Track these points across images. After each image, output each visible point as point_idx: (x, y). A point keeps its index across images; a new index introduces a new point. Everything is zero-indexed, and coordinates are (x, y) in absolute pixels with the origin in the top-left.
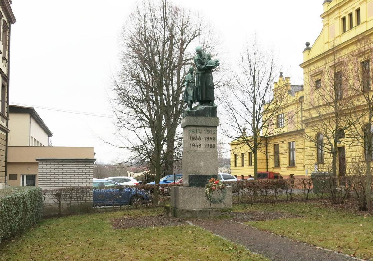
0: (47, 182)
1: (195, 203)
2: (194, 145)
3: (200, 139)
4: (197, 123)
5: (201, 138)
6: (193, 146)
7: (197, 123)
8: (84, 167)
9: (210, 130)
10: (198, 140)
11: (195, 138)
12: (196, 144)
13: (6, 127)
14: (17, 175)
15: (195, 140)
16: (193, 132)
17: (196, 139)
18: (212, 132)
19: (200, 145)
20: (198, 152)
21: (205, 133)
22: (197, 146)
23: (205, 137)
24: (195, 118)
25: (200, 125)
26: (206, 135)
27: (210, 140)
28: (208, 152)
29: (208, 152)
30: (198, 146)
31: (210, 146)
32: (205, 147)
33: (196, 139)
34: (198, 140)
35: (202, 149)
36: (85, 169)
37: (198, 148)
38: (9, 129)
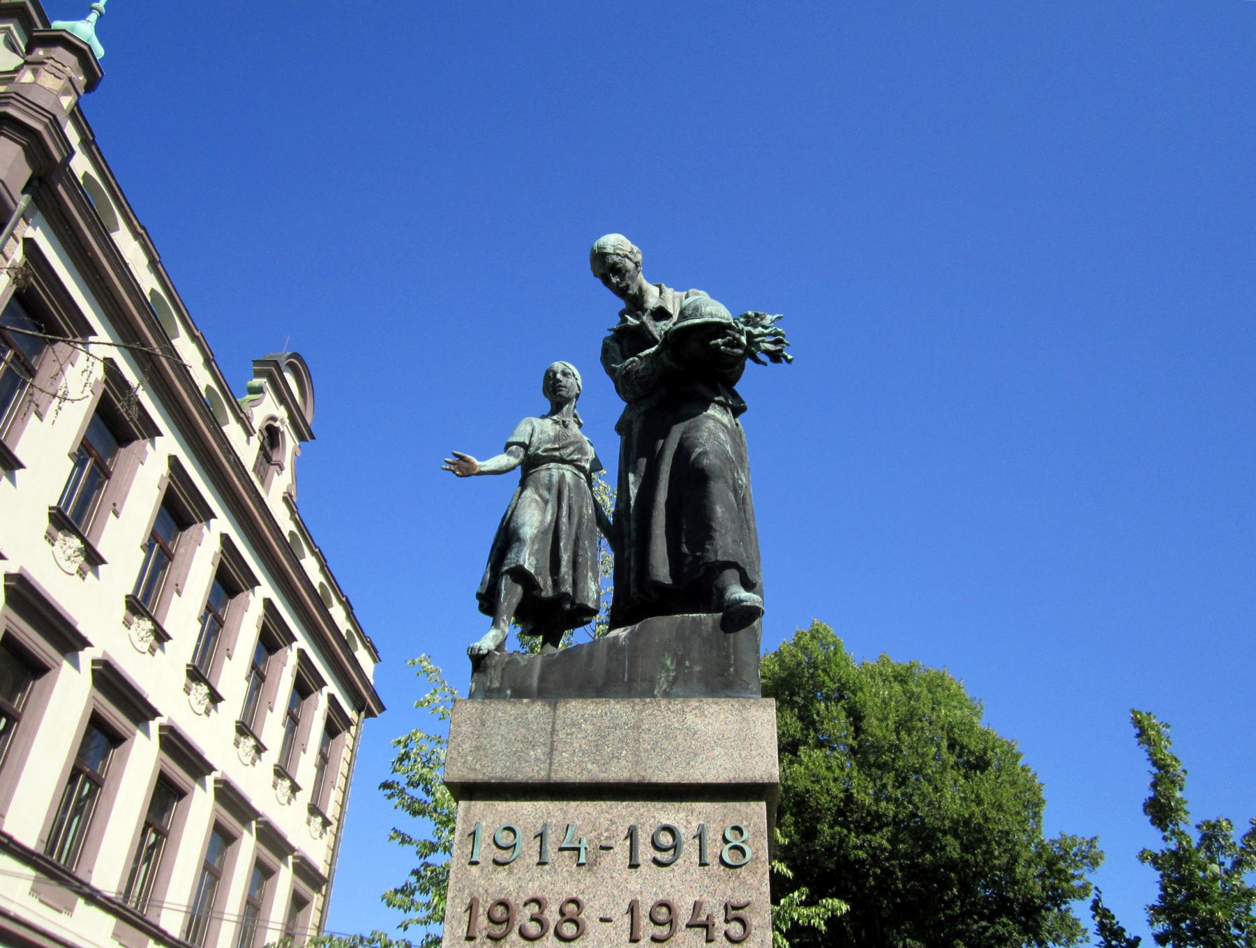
4: (550, 754)
5: (590, 915)
7: (550, 754)
9: (687, 833)
11: (524, 915)
15: (523, 934)
16: (503, 856)
17: (533, 929)
18: (714, 848)
23: (632, 909)
24: (536, 710)
25: (583, 777)
26: (648, 885)
33: (533, 929)
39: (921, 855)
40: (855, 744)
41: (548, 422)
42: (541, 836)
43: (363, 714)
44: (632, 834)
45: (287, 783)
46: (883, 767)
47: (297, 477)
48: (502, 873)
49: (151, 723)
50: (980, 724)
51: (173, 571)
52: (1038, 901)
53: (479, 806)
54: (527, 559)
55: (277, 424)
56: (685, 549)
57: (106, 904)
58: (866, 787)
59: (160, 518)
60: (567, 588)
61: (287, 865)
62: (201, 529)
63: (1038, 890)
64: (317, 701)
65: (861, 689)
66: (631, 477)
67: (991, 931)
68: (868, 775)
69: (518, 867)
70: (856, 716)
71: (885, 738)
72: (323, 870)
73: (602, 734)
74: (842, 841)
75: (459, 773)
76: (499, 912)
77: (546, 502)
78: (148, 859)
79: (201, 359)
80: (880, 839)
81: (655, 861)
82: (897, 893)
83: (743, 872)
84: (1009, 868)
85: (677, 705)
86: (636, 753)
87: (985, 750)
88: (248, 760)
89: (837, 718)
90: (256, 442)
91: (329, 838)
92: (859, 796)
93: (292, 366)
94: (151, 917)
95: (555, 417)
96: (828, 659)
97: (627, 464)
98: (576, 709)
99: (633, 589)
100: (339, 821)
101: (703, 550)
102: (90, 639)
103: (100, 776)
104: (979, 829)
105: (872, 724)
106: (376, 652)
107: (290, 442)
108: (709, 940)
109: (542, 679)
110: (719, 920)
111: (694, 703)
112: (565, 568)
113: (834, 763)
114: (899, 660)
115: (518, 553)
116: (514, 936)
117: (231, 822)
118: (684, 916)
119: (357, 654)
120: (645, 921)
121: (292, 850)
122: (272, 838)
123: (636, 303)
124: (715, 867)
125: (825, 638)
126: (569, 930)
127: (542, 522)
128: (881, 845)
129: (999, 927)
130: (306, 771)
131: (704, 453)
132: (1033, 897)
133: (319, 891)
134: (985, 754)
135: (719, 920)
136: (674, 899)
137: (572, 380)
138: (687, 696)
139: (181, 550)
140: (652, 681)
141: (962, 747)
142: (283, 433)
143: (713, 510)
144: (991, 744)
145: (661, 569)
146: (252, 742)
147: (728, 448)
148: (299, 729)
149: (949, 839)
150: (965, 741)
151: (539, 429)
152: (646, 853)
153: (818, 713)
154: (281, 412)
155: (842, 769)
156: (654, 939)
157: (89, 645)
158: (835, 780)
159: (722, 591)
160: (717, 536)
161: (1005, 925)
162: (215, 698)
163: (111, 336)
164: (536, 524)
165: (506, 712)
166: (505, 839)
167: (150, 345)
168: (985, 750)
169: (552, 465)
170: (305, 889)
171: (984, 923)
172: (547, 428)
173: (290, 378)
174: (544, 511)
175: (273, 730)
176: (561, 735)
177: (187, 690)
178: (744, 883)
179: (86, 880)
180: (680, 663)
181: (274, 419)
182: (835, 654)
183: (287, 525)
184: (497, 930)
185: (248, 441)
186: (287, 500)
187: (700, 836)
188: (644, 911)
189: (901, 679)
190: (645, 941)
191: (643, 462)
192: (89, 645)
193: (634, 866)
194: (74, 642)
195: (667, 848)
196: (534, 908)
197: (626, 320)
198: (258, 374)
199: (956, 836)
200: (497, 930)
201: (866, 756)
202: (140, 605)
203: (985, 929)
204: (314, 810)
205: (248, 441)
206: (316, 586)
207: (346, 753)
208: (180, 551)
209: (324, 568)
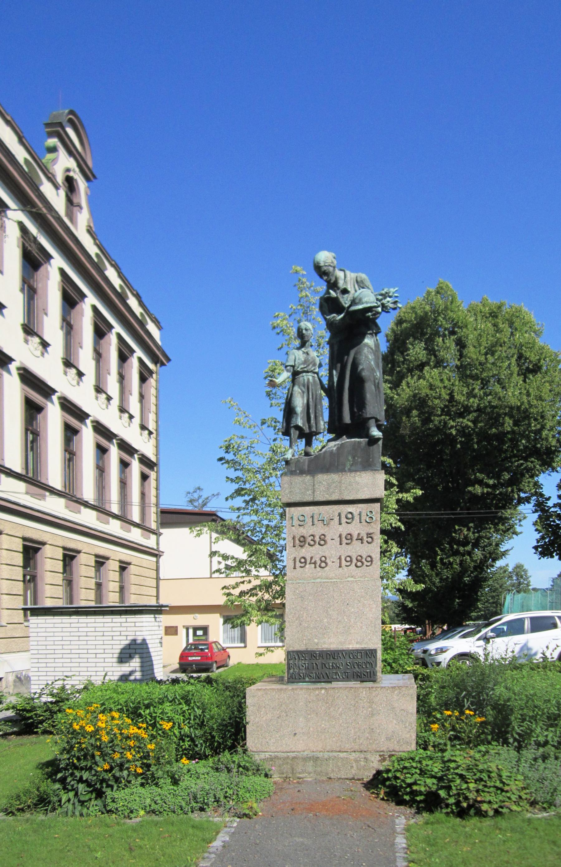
0: (48, 656)
1: (295, 734)
2: (305, 562)
3: (323, 540)
4: (313, 493)
5: (328, 538)
6: (348, 564)
7: (313, 493)
8: (123, 625)
9: (356, 514)
10: (317, 546)
11: (309, 539)
12: (312, 558)
13: (155, 548)
14: (177, 627)
15: (309, 544)
16: (302, 523)
17: (312, 543)
18: (364, 517)
19: (323, 559)
20: (319, 580)
21: (340, 524)
22: (315, 563)
23: (340, 536)
24: (308, 478)
25: (324, 499)
26: (344, 529)
27: (356, 544)
28: (349, 579)
29: (349, 579)
30: (317, 565)
31: (354, 561)
32: (340, 567)
33: (312, 543)
34: (317, 546)
35: (332, 570)
36: (125, 629)
37: (318, 569)
38: (161, 549)
39: (491, 428)
40: (459, 363)
41: (300, 352)
42: (312, 517)
43: (158, 365)
44: (339, 515)
45: (127, 415)
46: (475, 378)
47: (92, 213)
48: (301, 528)
49: (10, 366)
50: (540, 342)
51: (38, 301)
52: (553, 448)
53: (293, 509)
54: (300, 422)
55: (71, 174)
56: (356, 410)
57: (59, 494)
58: (463, 391)
59: (24, 268)
60: (314, 429)
61: (113, 444)
62: (47, 268)
63: (554, 443)
64: (132, 363)
65: (466, 326)
66: (334, 372)
67: (525, 465)
68: (464, 383)
69: (306, 526)
70: (461, 344)
71: (477, 359)
72: (153, 459)
73: (329, 485)
74: (445, 423)
75: (285, 500)
76: (302, 539)
77: (303, 392)
78: (32, 449)
79: (15, 139)
80: (466, 422)
81: (347, 522)
82: (474, 450)
83: (372, 524)
84: (538, 432)
85: (353, 474)
86: (340, 490)
87: (539, 360)
88: (75, 383)
89: (448, 348)
90: (62, 193)
91: (153, 441)
92: (457, 397)
93: (71, 122)
94: (107, 509)
95: (303, 349)
96: (446, 308)
97: (332, 367)
98: (321, 477)
99: (337, 423)
100: (156, 430)
101: (363, 412)
102: (13, 357)
103: (73, 451)
104: (526, 410)
105: (471, 352)
106: (159, 323)
107: (82, 184)
108: (362, 543)
109: (309, 466)
110: (365, 538)
111: (358, 473)
112: (313, 421)
113: (445, 378)
114: (493, 302)
115: (296, 419)
116: (307, 545)
117: (104, 442)
118: (355, 537)
119: (107, 273)
120: (344, 539)
121: (136, 451)
122: (125, 447)
123: (333, 285)
124: (364, 523)
125: (446, 292)
126: (322, 542)
127: (303, 403)
128: (467, 425)
129: (529, 463)
130: (134, 406)
131: (363, 369)
132: (551, 446)
133: (153, 470)
134: (539, 362)
135: (365, 538)
136: (352, 533)
137: (309, 332)
138: (356, 471)
139: (40, 285)
140: (344, 465)
141: (526, 359)
142: (76, 180)
143: (366, 396)
144: (543, 356)
145: (347, 418)
146: (104, 396)
147: (372, 363)
148: (125, 382)
149: (507, 418)
150: (528, 354)
151: (297, 356)
152: (344, 520)
153: (437, 346)
154: (71, 163)
155: (449, 380)
156: (347, 544)
157: (13, 360)
158: (445, 387)
159: (368, 429)
160: (367, 407)
161: (532, 462)
162: (80, 374)
163: (16, 204)
164: (301, 405)
165: (298, 480)
166: (301, 518)
167: (38, 206)
168: (539, 360)
169: (304, 374)
170: (146, 470)
171: (521, 462)
172: (299, 355)
173: (70, 131)
174: (303, 397)
175: (112, 386)
176: (317, 486)
177: (65, 373)
178: (372, 527)
179: (46, 483)
180: (354, 458)
181: (68, 170)
182: (452, 303)
183: (93, 250)
184: (302, 544)
185: (58, 194)
186: (89, 231)
187: (360, 514)
188: (343, 537)
189: (493, 315)
190: (344, 544)
191: (339, 365)
192: (13, 360)
193: (340, 524)
194: (83, 416)
195: (350, 518)
196: (312, 537)
197: (329, 293)
198: (51, 135)
199: (511, 416)
200: (302, 544)
201: (464, 371)
202: (29, 330)
203: (522, 464)
204: (143, 427)
205: (58, 194)
206: (21, 161)
207: (153, 391)
208: (39, 286)
209: (121, 275)
